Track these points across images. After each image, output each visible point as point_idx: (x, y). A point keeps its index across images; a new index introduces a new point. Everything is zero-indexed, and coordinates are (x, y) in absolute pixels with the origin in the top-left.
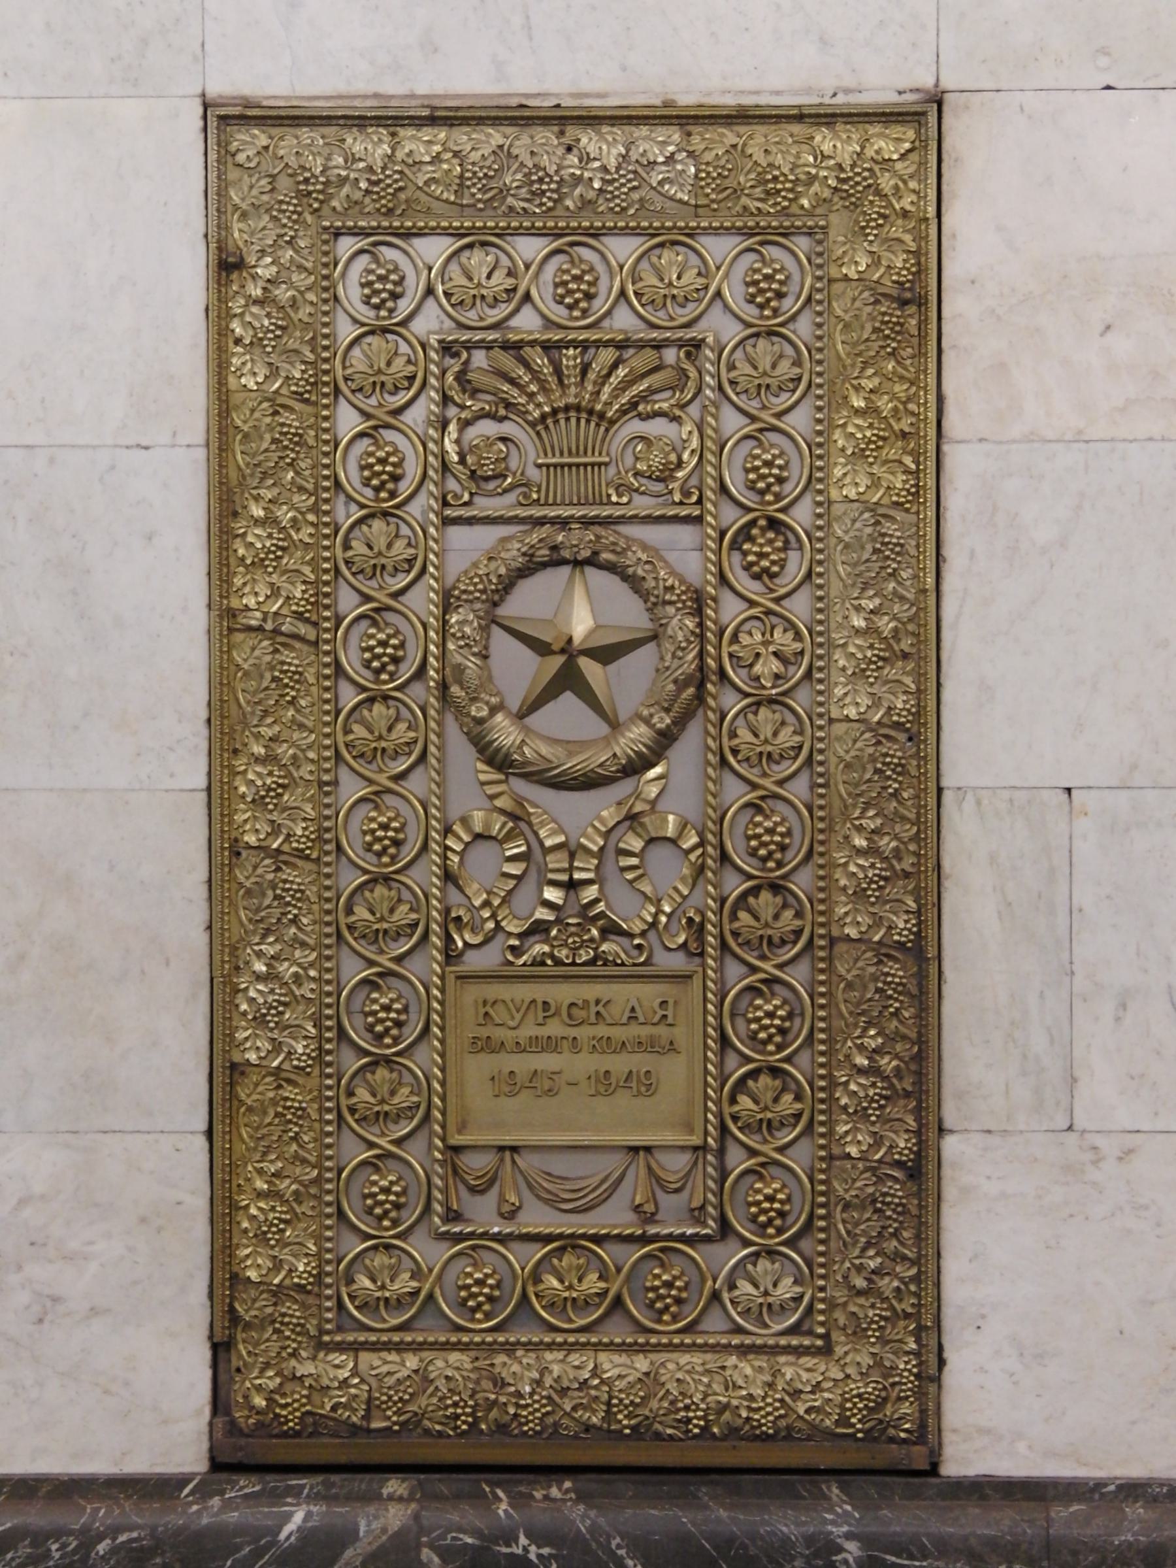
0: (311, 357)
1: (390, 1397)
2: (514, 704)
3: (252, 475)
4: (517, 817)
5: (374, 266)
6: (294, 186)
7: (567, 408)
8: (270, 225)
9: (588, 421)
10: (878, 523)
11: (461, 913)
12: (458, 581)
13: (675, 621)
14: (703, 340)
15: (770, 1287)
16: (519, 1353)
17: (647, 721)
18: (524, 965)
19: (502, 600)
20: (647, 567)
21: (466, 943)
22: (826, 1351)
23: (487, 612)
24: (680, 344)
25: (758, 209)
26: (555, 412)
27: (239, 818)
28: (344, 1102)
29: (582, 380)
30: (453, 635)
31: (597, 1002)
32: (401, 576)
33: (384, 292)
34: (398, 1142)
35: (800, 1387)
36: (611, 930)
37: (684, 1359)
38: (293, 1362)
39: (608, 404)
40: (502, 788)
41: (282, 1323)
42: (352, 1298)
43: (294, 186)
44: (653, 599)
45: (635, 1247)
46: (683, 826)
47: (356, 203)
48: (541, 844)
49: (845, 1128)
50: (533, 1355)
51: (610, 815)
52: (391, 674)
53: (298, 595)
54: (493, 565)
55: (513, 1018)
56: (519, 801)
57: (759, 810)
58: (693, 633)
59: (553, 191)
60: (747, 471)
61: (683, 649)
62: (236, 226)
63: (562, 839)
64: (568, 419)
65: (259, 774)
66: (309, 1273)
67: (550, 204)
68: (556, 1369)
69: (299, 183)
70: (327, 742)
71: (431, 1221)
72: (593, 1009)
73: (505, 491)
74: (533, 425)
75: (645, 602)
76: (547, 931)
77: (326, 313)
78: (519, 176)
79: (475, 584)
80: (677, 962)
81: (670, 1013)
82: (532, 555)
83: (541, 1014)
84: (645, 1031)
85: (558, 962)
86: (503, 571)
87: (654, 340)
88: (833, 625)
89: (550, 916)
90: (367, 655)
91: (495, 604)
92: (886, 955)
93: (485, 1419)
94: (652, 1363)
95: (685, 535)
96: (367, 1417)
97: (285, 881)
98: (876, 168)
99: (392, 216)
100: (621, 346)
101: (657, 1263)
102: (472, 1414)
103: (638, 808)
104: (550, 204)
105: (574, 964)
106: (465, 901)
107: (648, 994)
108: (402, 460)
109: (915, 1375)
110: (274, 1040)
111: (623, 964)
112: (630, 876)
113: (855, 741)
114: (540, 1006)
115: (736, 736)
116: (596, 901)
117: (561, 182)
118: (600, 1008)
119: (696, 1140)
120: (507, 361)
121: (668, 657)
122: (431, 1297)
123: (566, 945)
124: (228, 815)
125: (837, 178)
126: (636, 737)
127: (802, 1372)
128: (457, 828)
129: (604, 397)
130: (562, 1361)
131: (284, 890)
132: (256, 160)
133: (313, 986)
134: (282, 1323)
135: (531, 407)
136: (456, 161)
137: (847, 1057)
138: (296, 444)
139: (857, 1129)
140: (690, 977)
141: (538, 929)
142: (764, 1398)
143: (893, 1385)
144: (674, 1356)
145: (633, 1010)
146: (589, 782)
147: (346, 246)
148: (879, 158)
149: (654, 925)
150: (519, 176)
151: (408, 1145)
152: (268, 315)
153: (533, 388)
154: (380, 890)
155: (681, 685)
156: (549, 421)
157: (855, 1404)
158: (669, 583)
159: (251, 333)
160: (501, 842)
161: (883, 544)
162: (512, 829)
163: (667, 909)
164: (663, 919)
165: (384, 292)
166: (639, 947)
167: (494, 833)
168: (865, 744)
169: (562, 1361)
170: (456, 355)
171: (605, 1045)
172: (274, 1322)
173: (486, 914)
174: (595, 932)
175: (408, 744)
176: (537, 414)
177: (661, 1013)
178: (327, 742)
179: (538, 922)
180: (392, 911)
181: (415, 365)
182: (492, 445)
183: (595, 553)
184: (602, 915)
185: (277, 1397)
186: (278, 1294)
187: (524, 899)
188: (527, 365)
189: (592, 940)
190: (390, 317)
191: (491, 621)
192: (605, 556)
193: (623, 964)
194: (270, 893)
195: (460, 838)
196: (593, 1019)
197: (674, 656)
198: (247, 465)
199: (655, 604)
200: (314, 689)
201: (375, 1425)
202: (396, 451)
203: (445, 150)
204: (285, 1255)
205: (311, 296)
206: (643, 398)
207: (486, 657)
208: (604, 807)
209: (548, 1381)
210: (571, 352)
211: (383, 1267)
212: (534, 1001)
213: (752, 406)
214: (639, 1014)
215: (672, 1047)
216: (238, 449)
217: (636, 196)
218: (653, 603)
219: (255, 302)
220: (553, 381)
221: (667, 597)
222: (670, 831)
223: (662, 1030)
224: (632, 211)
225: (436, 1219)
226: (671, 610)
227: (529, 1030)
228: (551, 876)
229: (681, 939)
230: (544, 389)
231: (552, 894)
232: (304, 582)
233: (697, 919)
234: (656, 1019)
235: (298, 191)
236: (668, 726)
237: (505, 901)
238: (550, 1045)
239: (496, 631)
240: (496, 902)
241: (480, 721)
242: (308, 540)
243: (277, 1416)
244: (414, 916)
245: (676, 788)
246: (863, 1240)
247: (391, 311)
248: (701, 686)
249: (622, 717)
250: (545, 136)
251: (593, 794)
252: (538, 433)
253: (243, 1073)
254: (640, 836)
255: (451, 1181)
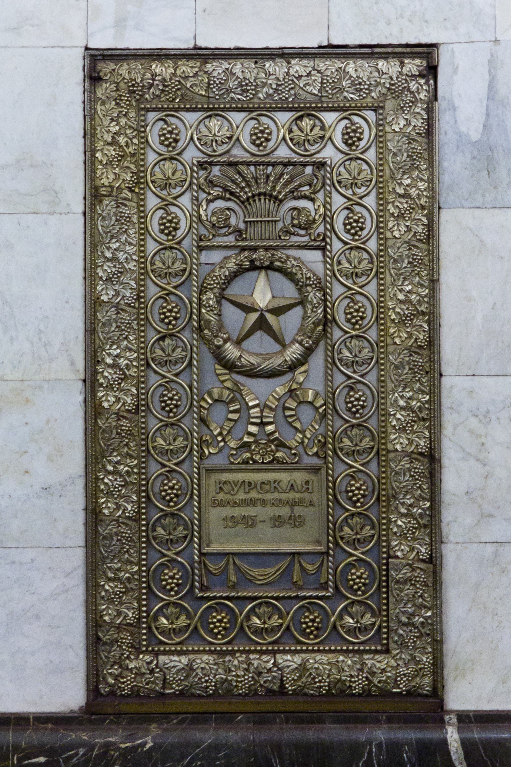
0: (135, 170)
1: (174, 679)
2: (234, 337)
3: (106, 237)
4: (237, 389)
5: (165, 126)
6: (127, 86)
7: (260, 194)
8: (116, 107)
9: (270, 200)
10: (409, 143)
11: (208, 438)
12: (205, 279)
13: (311, 294)
14: (325, 162)
15: (358, 442)
16: (238, 655)
17: (300, 343)
18: (238, 463)
19: (227, 287)
20: (297, 268)
21: (210, 453)
22: (387, 651)
23: (220, 294)
24: (313, 164)
25: (352, 98)
26: (253, 196)
27: (99, 288)
28: (150, 534)
29: (267, 181)
30: (205, 305)
31: (275, 482)
32: (178, 278)
33: (170, 139)
34: (177, 375)
35: (375, 670)
36: (281, 445)
37: (319, 657)
38: (127, 662)
39: (280, 192)
40: (227, 377)
41: (122, 642)
42: (157, 629)
43: (127, 86)
44: (301, 284)
45: (294, 602)
46: (316, 395)
47: (157, 96)
48: (247, 404)
49: (396, 543)
50: (244, 656)
51: (281, 390)
52: (175, 413)
53: (128, 295)
54: (223, 270)
55: (233, 490)
56: (236, 383)
57: (353, 478)
58: (321, 299)
59: (252, 90)
60: (346, 314)
61: (316, 307)
62: (99, 224)
63: (257, 402)
64: (260, 200)
65: (109, 266)
66: (134, 511)
67: (251, 96)
68: (256, 663)
69: (129, 86)
70: (143, 357)
71: (194, 592)
72: (273, 485)
73: (230, 234)
74: (243, 203)
75: (297, 285)
76: (250, 446)
77: (142, 149)
78: (236, 83)
79: (214, 281)
80: (315, 461)
81: (310, 487)
82: (241, 265)
83: (247, 488)
84: (297, 496)
85: (255, 462)
86: (227, 273)
87: (301, 162)
88: (388, 298)
89: (251, 439)
90: (162, 227)
91: (224, 290)
92: (415, 459)
93: (221, 687)
94: (303, 660)
95: (317, 255)
96: (164, 688)
97: (122, 319)
98: (408, 79)
99: (175, 100)
100: (286, 165)
101: (305, 609)
102: (215, 686)
103: (294, 386)
104: (251, 96)
105: (263, 463)
106: (209, 432)
107: (299, 477)
108: (179, 221)
109: (432, 664)
110: (115, 290)
111: (287, 463)
112: (290, 420)
113: (399, 354)
114: (247, 484)
115: (340, 175)
116: (274, 432)
117: (257, 86)
118: (276, 484)
119: (323, 549)
120: (231, 172)
121: (309, 311)
122: (196, 628)
123: (259, 453)
124: (93, 171)
125: (390, 83)
126: (294, 351)
127: (376, 663)
128: (206, 397)
129: (278, 188)
130: (258, 659)
131: (121, 323)
132: (109, 75)
133: (135, 370)
134: (122, 642)
135: (242, 194)
136: (205, 76)
137: (396, 508)
138: (128, 328)
139: (400, 437)
140: (320, 469)
141: (246, 446)
142: (357, 677)
143: (421, 669)
144: (313, 655)
145: (292, 486)
146: (271, 374)
147: (152, 116)
148: (410, 74)
149: (302, 442)
150: (236, 83)
151: (182, 376)
152: (114, 150)
153: (243, 184)
154: (169, 430)
155: (316, 324)
156: (251, 200)
157: (402, 679)
158: (308, 275)
159: (106, 158)
160: (228, 403)
161: (413, 259)
162: (233, 397)
163: (309, 436)
164: (306, 441)
165: (170, 139)
166: (295, 454)
167: (224, 399)
168: (404, 356)
169: (258, 659)
170: (206, 169)
171: (279, 503)
172: (117, 642)
173: (219, 438)
174: (273, 447)
175: (182, 358)
176: (245, 197)
177: (306, 487)
178: (143, 357)
179: (246, 442)
180: (173, 351)
181: (186, 264)
182: (223, 212)
183: (272, 263)
184: (277, 439)
185: (119, 678)
186: (119, 628)
187: (238, 431)
188: (239, 173)
189: (272, 451)
190: (173, 329)
191: (221, 298)
192: (277, 264)
193: (287, 463)
194: (114, 325)
195: (208, 402)
196: (272, 490)
197: (312, 311)
198: (104, 338)
199: (301, 286)
200: (137, 438)
201: (167, 691)
202: (176, 217)
203: (200, 70)
204: (121, 502)
205: (135, 141)
206: (296, 189)
207: (220, 315)
208: (279, 387)
209: (252, 669)
210: (261, 167)
211: (172, 613)
212: (244, 482)
213: (349, 193)
214: (295, 487)
215: (311, 504)
216: (100, 330)
217: (292, 92)
218: (300, 286)
219: (108, 144)
220: (253, 183)
221: (308, 282)
222: (310, 399)
223: (305, 495)
224: (291, 99)
225: (197, 591)
226: (309, 289)
227: (241, 496)
228: (252, 420)
229: (315, 450)
230: (249, 185)
231: (253, 429)
232: (131, 289)
233: (323, 440)
234: (304, 489)
235: (129, 90)
236: (311, 345)
237: (229, 432)
238: (251, 503)
239: (224, 302)
240: (225, 433)
241: (219, 347)
242: (133, 268)
243: (119, 687)
244: (186, 532)
245: (313, 378)
246: (406, 599)
247: (174, 148)
248: (325, 325)
249: (288, 341)
250: (249, 64)
251: (271, 380)
252: (246, 207)
253: (100, 305)
254: (295, 400)
255: (203, 571)
